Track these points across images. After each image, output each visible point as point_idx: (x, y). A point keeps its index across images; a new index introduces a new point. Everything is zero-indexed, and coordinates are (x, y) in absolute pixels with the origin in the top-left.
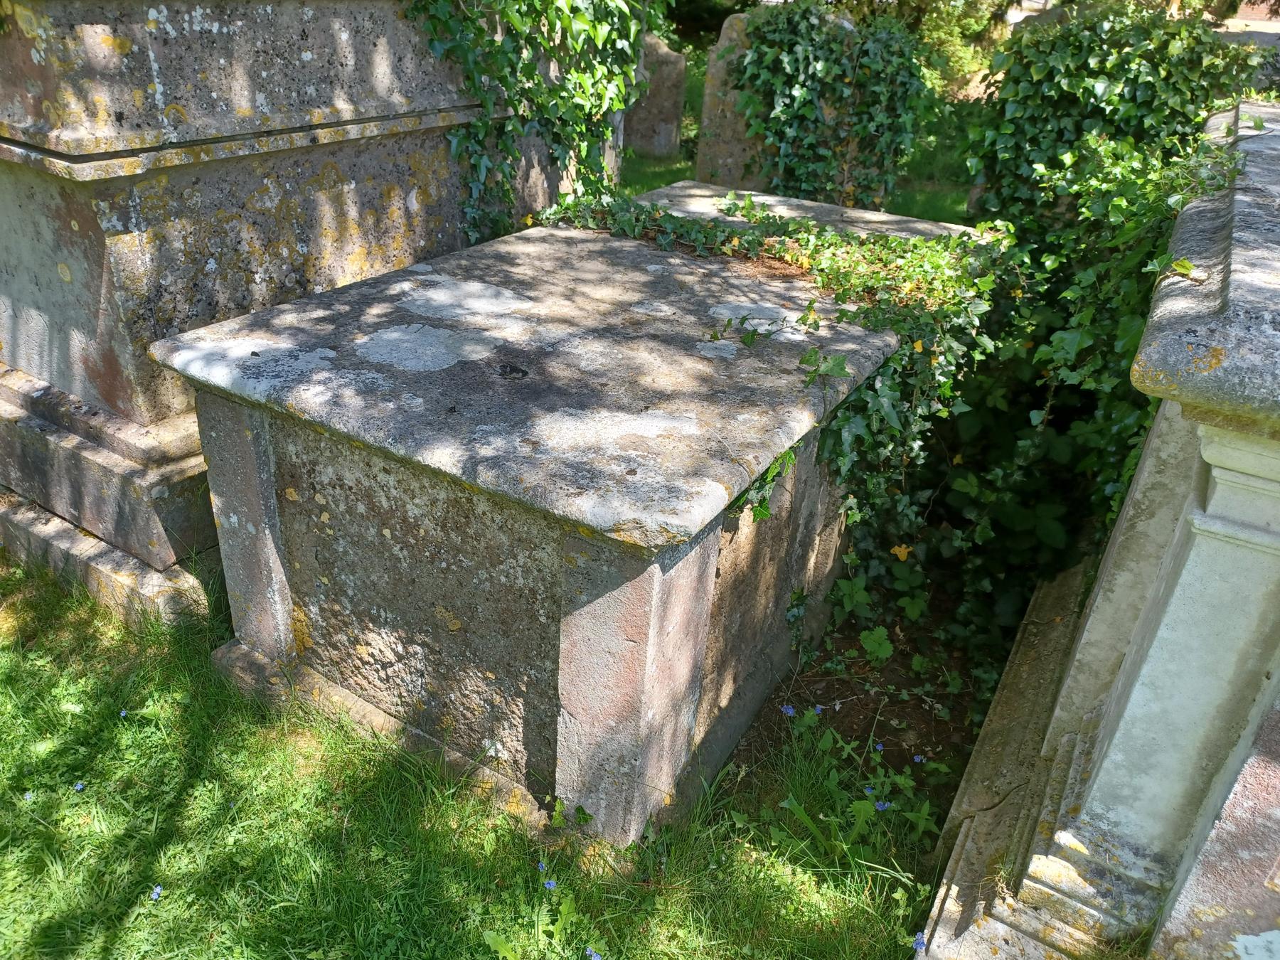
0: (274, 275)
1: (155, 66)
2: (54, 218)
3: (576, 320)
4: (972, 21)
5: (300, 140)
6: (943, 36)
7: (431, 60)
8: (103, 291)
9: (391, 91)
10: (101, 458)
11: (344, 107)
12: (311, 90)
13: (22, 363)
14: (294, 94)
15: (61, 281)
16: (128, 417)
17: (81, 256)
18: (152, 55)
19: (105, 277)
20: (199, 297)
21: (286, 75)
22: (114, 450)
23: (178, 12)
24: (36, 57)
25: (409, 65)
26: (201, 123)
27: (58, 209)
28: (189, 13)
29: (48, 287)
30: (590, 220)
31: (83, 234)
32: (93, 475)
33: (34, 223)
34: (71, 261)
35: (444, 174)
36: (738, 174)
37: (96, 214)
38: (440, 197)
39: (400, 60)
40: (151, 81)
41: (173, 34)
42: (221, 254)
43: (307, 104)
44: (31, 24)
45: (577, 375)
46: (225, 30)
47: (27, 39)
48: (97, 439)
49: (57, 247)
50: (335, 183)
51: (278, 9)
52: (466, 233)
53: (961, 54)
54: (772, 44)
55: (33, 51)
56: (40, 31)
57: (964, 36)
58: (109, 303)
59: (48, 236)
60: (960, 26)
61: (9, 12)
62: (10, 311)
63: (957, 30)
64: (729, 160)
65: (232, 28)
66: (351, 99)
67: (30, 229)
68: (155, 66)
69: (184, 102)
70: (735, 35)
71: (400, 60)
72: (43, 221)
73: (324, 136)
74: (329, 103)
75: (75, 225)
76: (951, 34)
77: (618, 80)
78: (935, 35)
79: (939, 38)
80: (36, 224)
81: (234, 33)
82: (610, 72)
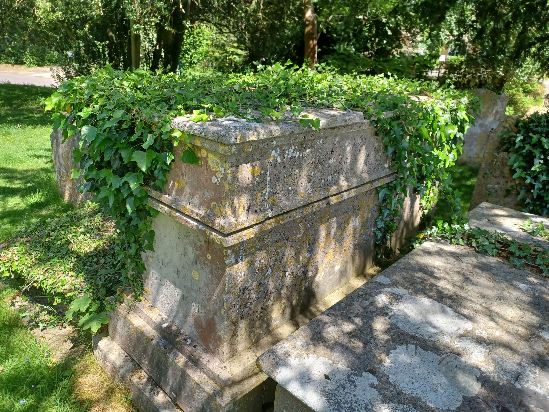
0: (294, 271)
1: (269, 179)
2: (197, 250)
3: (513, 346)
4: (529, 85)
5: (323, 204)
6: (515, 92)
7: (380, 154)
8: (217, 291)
9: (362, 172)
10: (196, 376)
11: (344, 184)
12: (330, 178)
13: (159, 305)
14: (323, 181)
15: (192, 279)
16: (212, 352)
17: (208, 271)
18: (268, 173)
19: (220, 285)
20: (260, 289)
21: (321, 172)
22: (204, 372)
23: (284, 150)
24: (214, 180)
25: (372, 157)
26: (285, 204)
27: (201, 246)
28: (288, 149)
29: (184, 277)
30: (461, 240)
31: (213, 262)
32: (190, 385)
33: (185, 248)
34: (201, 271)
35: (371, 206)
36: (501, 194)
37: (225, 256)
38: (368, 217)
39: (368, 156)
40: (266, 187)
41: (279, 161)
42: (274, 265)
43: (328, 185)
44: (217, 164)
45: (357, 251)
46: (301, 155)
47: (211, 171)
48: (194, 362)
49: (195, 262)
50: (328, 219)
51: (325, 140)
52: (375, 234)
53: (524, 100)
54: (535, 133)
55: (214, 177)
56: (222, 169)
57: (524, 92)
58: (219, 297)
59: (191, 255)
60: (522, 88)
61: (205, 156)
62: (158, 281)
63: (521, 89)
64: (496, 186)
65: (304, 153)
66: (347, 180)
67: (181, 250)
68: (269, 179)
69: (277, 194)
70: (507, 125)
71: (368, 156)
72: (190, 249)
73: (333, 200)
74: (337, 183)
75: (209, 257)
76: (518, 91)
77: (454, 152)
78: (510, 91)
79: (512, 93)
80: (185, 249)
81: (305, 156)
82: (451, 148)
